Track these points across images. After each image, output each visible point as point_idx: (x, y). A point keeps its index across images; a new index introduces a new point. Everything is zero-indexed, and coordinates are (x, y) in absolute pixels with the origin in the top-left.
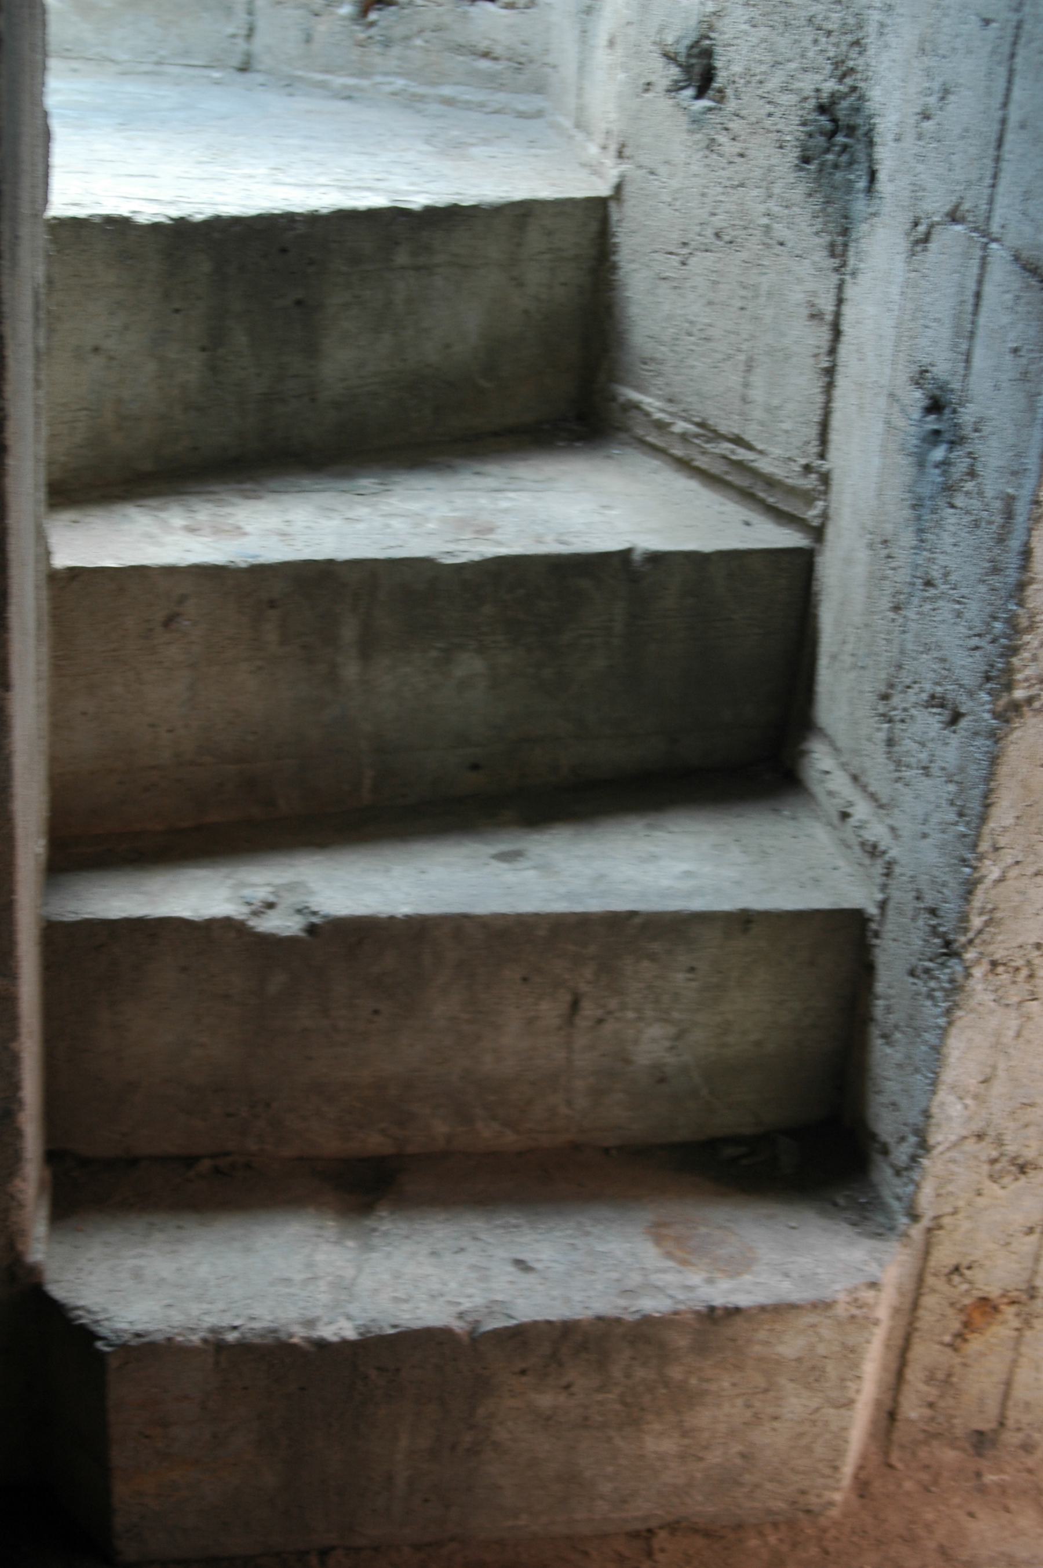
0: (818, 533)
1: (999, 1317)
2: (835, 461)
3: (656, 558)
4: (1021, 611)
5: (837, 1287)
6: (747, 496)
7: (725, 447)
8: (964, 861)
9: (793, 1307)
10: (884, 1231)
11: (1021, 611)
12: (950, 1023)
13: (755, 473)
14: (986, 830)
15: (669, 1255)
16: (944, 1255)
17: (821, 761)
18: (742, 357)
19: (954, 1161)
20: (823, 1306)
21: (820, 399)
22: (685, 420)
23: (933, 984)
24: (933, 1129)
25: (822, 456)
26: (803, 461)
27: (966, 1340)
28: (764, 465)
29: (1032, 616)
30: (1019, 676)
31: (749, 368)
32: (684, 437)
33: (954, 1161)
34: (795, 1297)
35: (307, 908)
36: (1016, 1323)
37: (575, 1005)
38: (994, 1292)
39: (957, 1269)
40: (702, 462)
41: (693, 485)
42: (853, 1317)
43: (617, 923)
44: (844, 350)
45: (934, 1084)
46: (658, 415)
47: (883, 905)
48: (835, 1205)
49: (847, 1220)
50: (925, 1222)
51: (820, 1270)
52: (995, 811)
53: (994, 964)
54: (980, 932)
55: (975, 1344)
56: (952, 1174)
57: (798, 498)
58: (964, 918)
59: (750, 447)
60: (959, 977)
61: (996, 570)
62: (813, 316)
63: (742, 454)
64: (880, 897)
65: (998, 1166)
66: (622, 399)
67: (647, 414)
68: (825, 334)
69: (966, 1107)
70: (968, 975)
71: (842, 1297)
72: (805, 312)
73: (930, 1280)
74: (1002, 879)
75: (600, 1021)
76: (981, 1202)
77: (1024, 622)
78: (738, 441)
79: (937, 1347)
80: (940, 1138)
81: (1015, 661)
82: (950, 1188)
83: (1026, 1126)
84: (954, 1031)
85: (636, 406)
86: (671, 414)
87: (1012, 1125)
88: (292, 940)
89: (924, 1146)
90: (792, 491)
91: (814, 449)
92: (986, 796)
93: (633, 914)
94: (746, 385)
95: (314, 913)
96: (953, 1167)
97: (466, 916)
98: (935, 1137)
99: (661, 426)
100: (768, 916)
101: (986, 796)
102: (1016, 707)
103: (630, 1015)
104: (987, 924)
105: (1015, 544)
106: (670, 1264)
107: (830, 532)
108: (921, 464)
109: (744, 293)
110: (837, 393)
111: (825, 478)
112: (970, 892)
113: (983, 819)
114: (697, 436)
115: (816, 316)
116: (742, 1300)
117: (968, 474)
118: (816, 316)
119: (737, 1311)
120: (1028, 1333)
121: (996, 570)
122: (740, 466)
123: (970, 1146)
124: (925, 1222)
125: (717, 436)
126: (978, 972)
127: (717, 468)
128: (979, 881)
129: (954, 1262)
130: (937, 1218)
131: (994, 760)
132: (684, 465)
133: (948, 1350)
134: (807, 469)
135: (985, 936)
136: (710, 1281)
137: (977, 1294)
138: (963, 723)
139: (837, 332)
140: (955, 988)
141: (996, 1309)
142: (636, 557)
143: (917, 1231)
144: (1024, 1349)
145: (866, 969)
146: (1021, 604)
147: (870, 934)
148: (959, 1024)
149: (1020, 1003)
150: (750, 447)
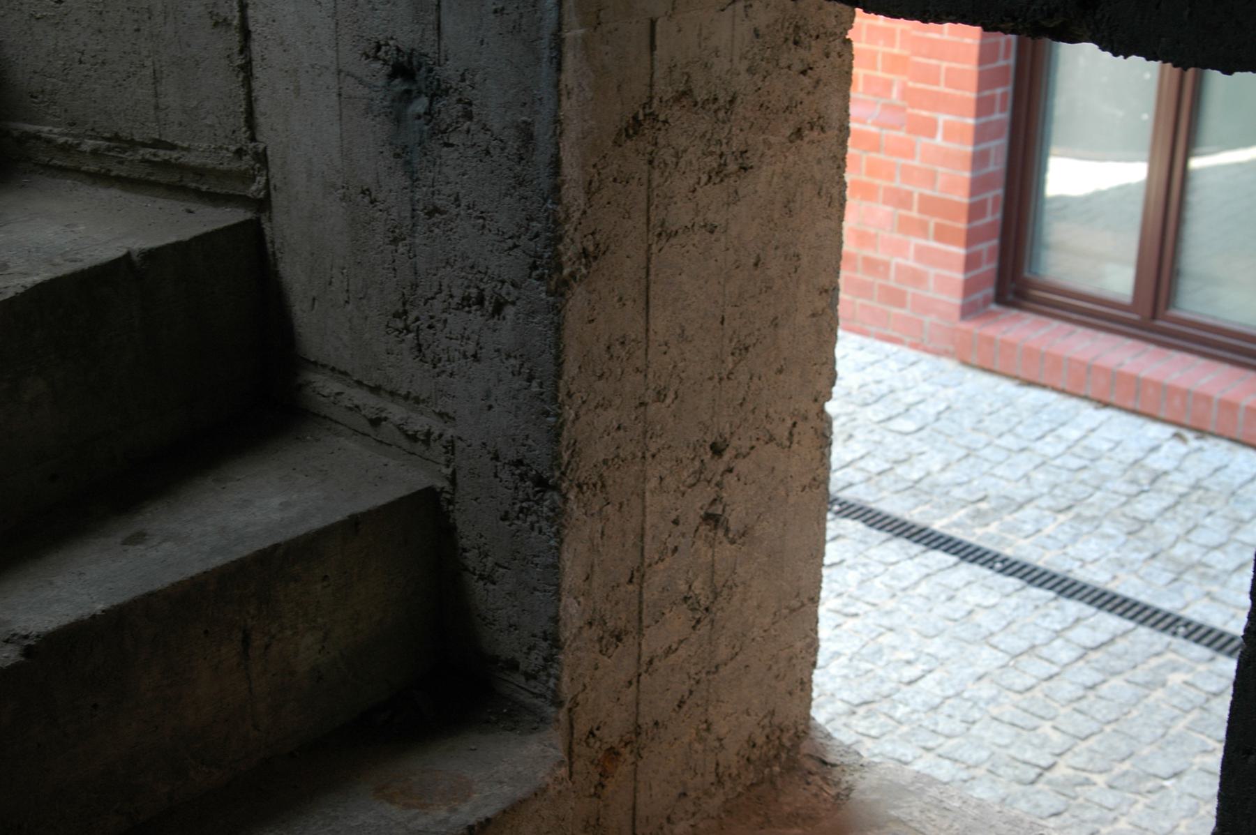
0: (263, 204)
1: (622, 759)
2: (268, 137)
3: (151, 255)
4: (559, 208)
5: (541, 775)
6: (176, 190)
7: (147, 153)
8: (547, 414)
9: (522, 802)
10: (539, 722)
11: (559, 208)
12: (562, 541)
13: (183, 168)
14: (561, 383)
15: (408, 806)
16: (582, 727)
17: (324, 385)
18: (148, 72)
19: (578, 649)
20: (540, 792)
21: (242, 93)
22: (91, 138)
23: (533, 518)
24: (562, 629)
25: (253, 139)
26: (233, 148)
27: (603, 786)
28: (191, 159)
29: (566, 212)
30: (564, 258)
31: (156, 80)
32: (95, 152)
33: (578, 649)
34: (520, 794)
35: (14, 635)
36: (631, 759)
37: (246, 641)
38: (614, 740)
39: (591, 733)
40: (123, 171)
41: (115, 192)
42: (560, 792)
43: (264, 558)
44: (256, 48)
45: (558, 594)
46: (62, 140)
47: (453, 480)
48: (488, 722)
49: (504, 729)
50: (567, 705)
51: (520, 769)
52: (567, 366)
53: (580, 486)
54: (569, 463)
55: (611, 786)
56: (579, 659)
57: (244, 179)
58: (556, 457)
59: (173, 147)
60: (559, 503)
61: (521, 182)
62: (216, 24)
63: (163, 154)
64: (449, 471)
65: (604, 642)
66: (16, 134)
67: (49, 141)
68: (235, 38)
69: (579, 603)
70: (566, 499)
71: (549, 780)
72: (210, 22)
73: (576, 748)
74: (577, 417)
75: (267, 647)
76: (598, 674)
77: (563, 216)
78: (157, 144)
79: (587, 800)
80: (567, 634)
81: (561, 247)
82: (579, 671)
83: (617, 604)
84: (565, 546)
85: (37, 136)
86: (74, 136)
87: (608, 606)
88: (15, 667)
89: (555, 642)
90: (227, 175)
91: (243, 134)
92: (557, 357)
93: (276, 547)
94: (156, 95)
95: (26, 637)
96: (578, 654)
97: (151, 594)
98: (566, 634)
99: (66, 149)
100: (369, 514)
101: (557, 357)
102: (565, 283)
103: (289, 633)
104: (572, 456)
105: (542, 158)
106: (414, 811)
107: (277, 200)
108: (398, 120)
109: (136, 16)
110: (256, 85)
111: (262, 158)
112: (558, 435)
113: (558, 376)
114: (109, 149)
115: (221, 23)
116: (488, 812)
117: (463, 116)
118: (221, 23)
119: (488, 820)
120: (640, 763)
121: (521, 182)
122: (166, 164)
123: (587, 633)
124: (567, 705)
125: (133, 144)
126: (571, 496)
127: (140, 172)
128: (562, 425)
129: (588, 728)
130: (575, 697)
131: (558, 328)
132: (103, 178)
133: (595, 799)
134: (239, 153)
135: (573, 465)
136: (453, 810)
137: (605, 747)
138: (509, 311)
139: (246, 33)
140: (558, 515)
141: (618, 754)
142: (135, 258)
143: (563, 715)
144: (639, 777)
145: (449, 531)
146: (558, 201)
147: (444, 504)
148: (567, 540)
149: (601, 510)
150: (173, 147)
